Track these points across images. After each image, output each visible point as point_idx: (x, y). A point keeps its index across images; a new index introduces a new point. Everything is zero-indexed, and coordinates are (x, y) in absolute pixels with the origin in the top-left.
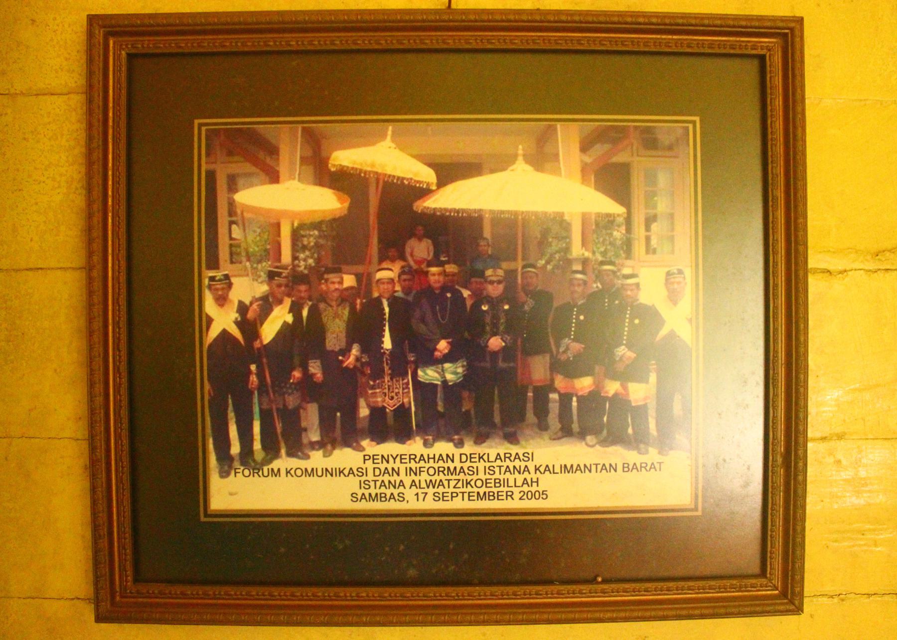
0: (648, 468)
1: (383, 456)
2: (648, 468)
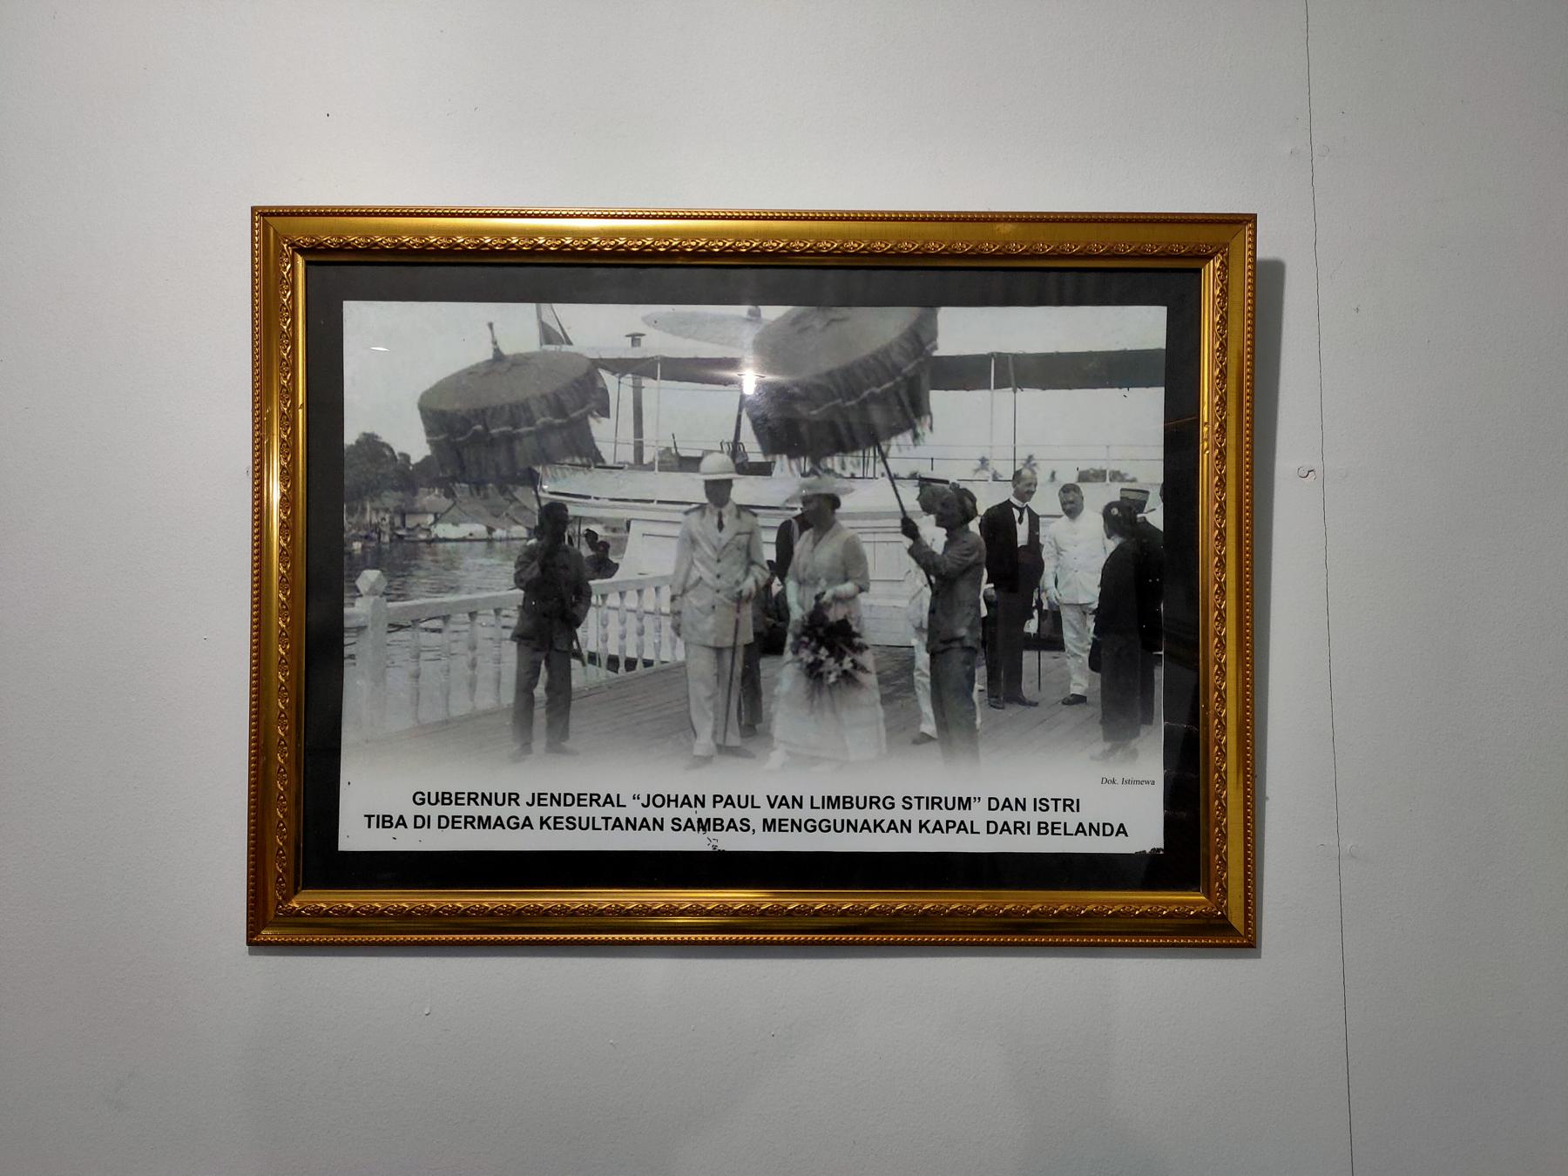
0: (601, 802)
1: (552, 796)
2: (601, 802)
